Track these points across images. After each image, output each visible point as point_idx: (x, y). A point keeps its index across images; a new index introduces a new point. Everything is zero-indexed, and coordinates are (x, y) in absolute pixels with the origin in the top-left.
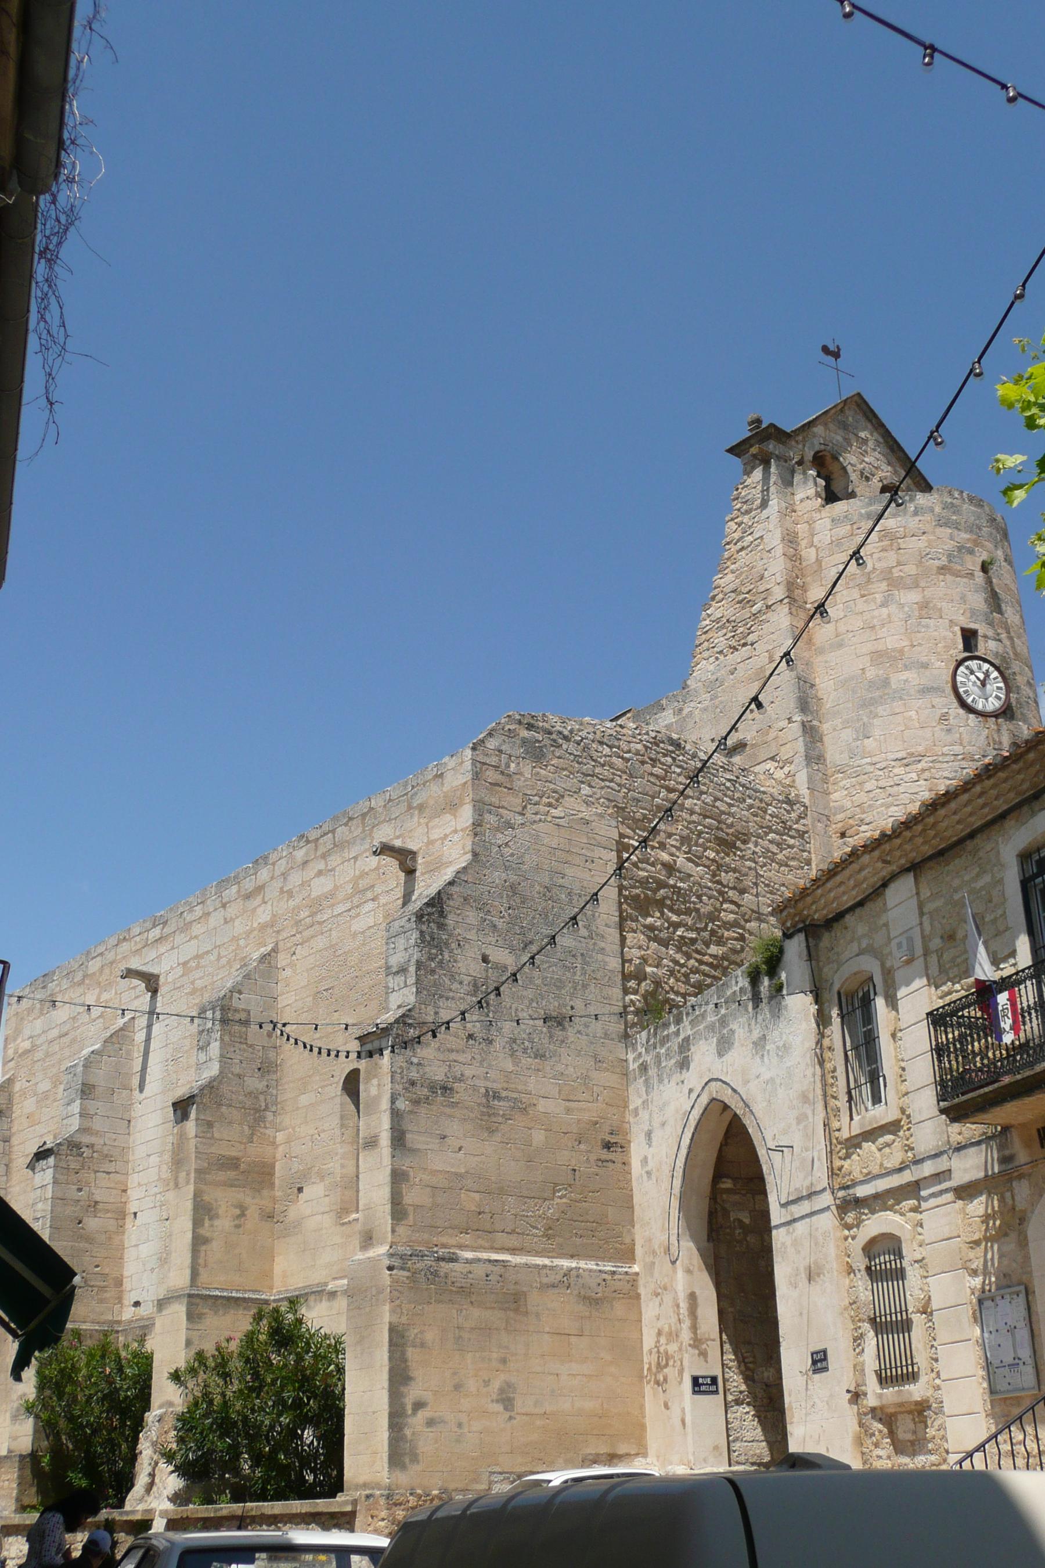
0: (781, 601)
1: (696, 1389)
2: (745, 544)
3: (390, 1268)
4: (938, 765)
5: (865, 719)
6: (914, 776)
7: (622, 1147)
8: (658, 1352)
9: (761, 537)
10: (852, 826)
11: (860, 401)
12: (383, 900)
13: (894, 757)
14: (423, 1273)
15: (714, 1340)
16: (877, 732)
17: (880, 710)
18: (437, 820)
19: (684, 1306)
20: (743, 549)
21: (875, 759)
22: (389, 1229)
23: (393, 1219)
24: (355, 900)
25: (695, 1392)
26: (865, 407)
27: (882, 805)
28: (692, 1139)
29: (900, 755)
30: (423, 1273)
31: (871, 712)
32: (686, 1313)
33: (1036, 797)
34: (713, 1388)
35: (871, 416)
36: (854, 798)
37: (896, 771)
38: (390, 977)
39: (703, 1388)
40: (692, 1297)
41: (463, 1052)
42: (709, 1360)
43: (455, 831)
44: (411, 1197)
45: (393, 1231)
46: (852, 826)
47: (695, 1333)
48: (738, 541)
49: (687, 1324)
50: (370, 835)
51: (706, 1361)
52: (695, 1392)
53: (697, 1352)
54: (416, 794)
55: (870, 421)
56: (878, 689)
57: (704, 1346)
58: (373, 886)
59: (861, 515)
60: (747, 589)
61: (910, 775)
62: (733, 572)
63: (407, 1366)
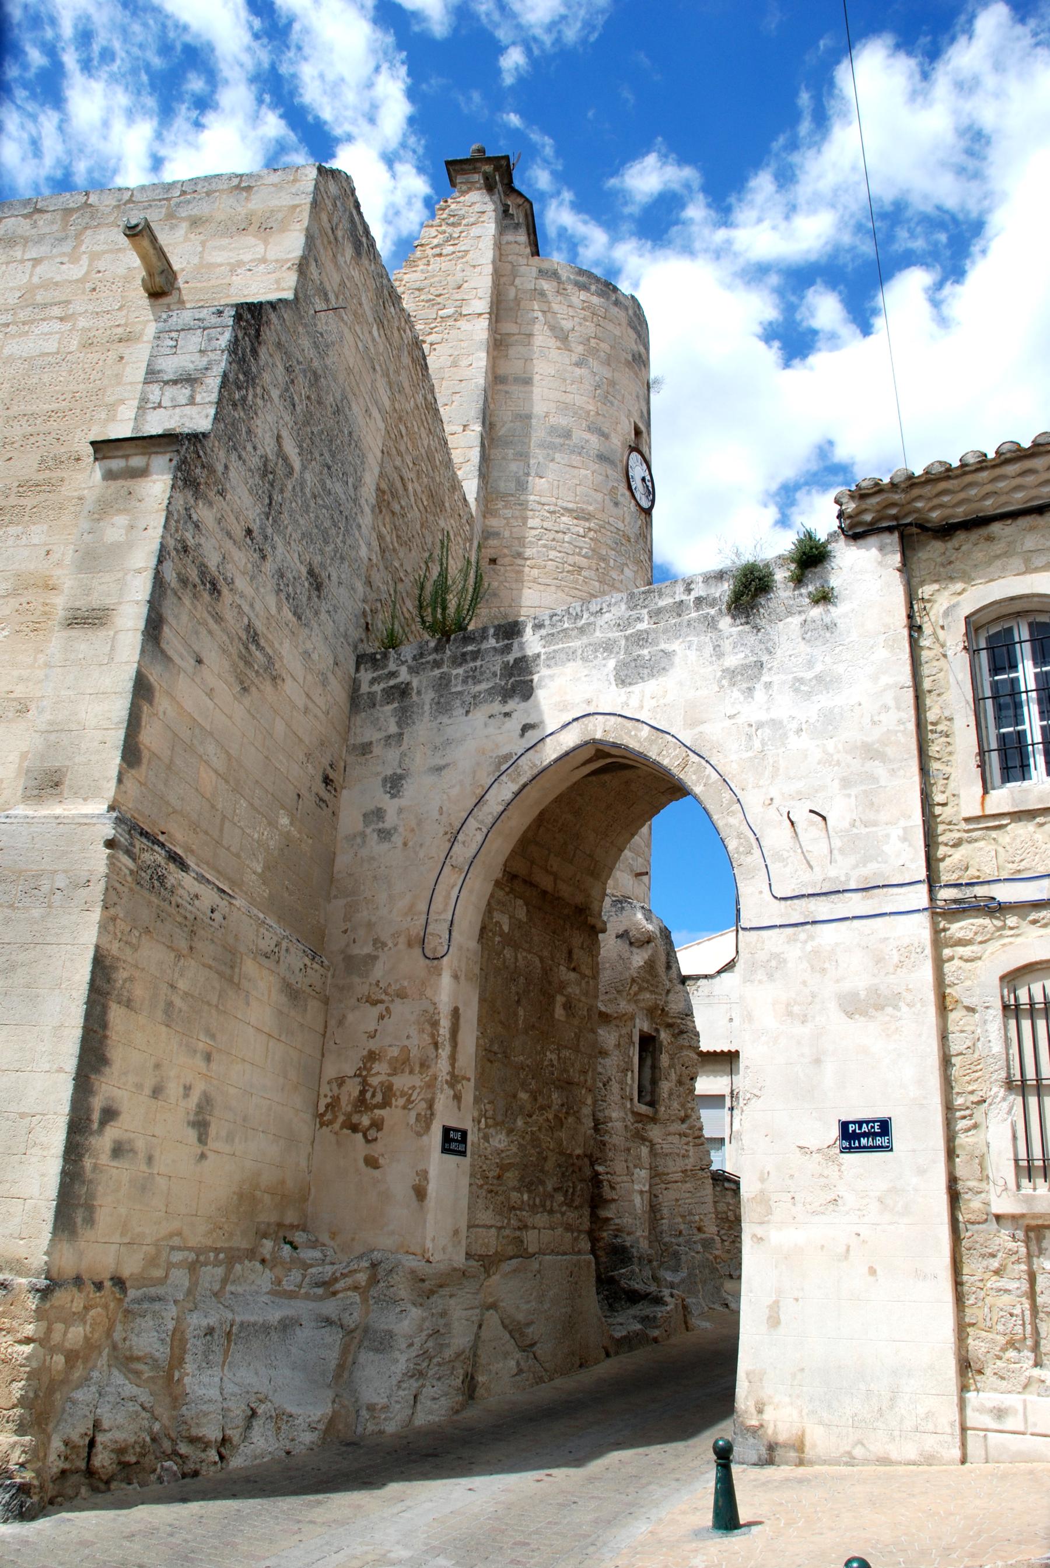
0: (480, 314)
1: (447, 1145)
2: (444, 252)
3: (110, 844)
4: (603, 530)
5: (541, 460)
6: (581, 531)
7: (335, 790)
8: (365, 1083)
9: (467, 252)
10: (505, 556)
11: (529, 212)
12: (82, 323)
13: (565, 504)
14: (149, 872)
15: (469, 1080)
16: (551, 476)
17: (558, 456)
18: (227, 241)
19: (445, 1024)
20: (440, 255)
21: (543, 500)
22: (114, 774)
23: (124, 758)
24: (22, 315)
25: (445, 1150)
26: (530, 218)
27: (545, 546)
28: (517, 794)
29: (571, 506)
30: (149, 872)
31: (548, 454)
32: (448, 1036)
33: (1039, 510)
34: (461, 1148)
35: (531, 231)
36: (514, 530)
37: (564, 519)
38: (155, 388)
39: (453, 1146)
40: (456, 1013)
41: (239, 548)
42: (462, 1106)
43: (264, 260)
44: (150, 737)
45: (120, 781)
46: (505, 556)
47: (453, 1065)
48: (436, 246)
49: (445, 1053)
50: (78, 236)
51: (459, 1108)
52: (445, 1150)
53: (452, 1093)
54: (189, 202)
55: (529, 234)
56: (559, 436)
57: (459, 1087)
58: (68, 302)
59: (569, 278)
60: (438, 293)
61: (577, 529)
62: (422, 271)
63: (105, 1037)
